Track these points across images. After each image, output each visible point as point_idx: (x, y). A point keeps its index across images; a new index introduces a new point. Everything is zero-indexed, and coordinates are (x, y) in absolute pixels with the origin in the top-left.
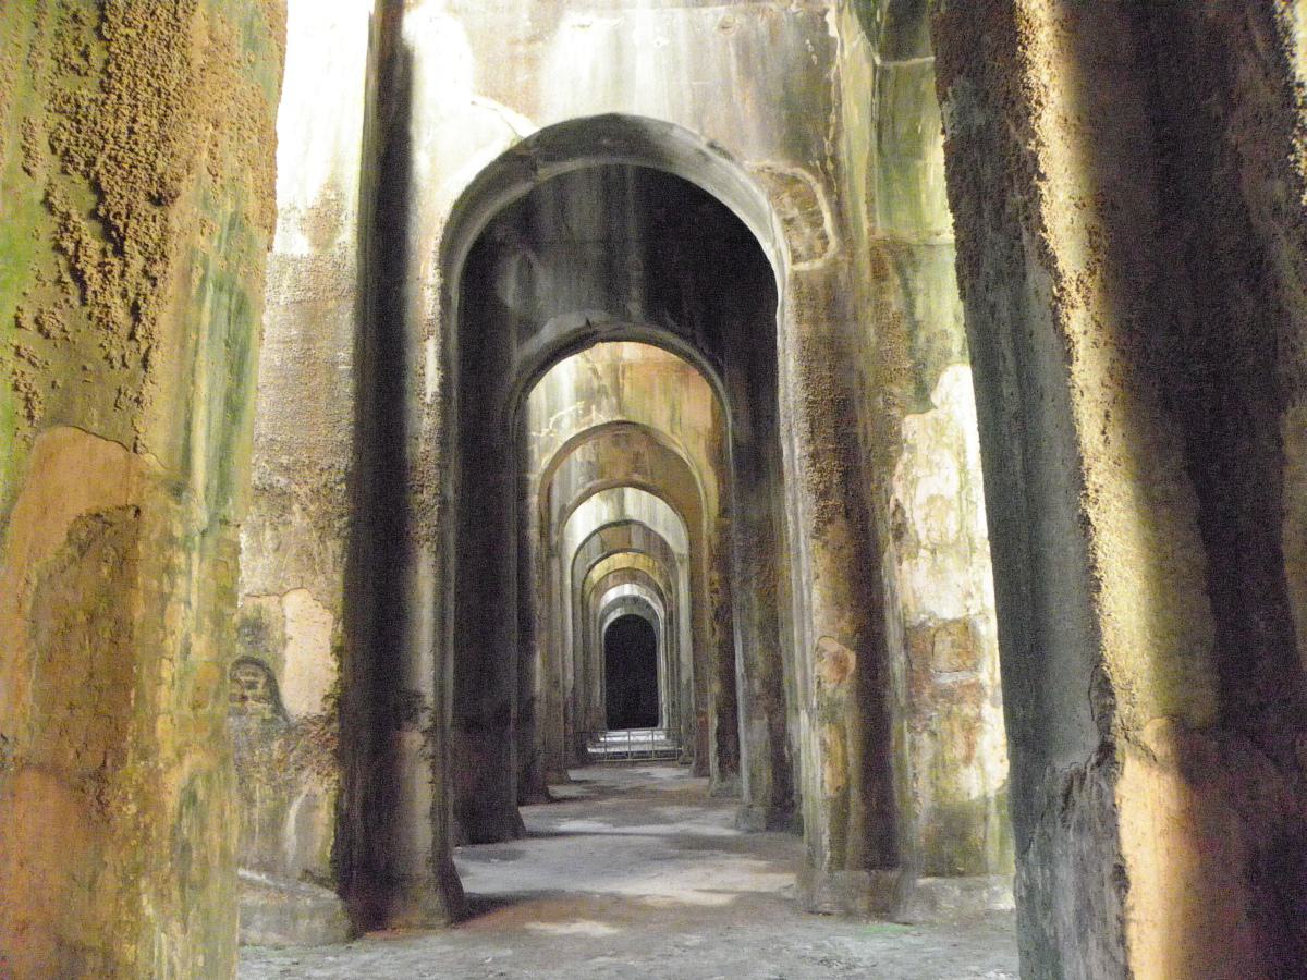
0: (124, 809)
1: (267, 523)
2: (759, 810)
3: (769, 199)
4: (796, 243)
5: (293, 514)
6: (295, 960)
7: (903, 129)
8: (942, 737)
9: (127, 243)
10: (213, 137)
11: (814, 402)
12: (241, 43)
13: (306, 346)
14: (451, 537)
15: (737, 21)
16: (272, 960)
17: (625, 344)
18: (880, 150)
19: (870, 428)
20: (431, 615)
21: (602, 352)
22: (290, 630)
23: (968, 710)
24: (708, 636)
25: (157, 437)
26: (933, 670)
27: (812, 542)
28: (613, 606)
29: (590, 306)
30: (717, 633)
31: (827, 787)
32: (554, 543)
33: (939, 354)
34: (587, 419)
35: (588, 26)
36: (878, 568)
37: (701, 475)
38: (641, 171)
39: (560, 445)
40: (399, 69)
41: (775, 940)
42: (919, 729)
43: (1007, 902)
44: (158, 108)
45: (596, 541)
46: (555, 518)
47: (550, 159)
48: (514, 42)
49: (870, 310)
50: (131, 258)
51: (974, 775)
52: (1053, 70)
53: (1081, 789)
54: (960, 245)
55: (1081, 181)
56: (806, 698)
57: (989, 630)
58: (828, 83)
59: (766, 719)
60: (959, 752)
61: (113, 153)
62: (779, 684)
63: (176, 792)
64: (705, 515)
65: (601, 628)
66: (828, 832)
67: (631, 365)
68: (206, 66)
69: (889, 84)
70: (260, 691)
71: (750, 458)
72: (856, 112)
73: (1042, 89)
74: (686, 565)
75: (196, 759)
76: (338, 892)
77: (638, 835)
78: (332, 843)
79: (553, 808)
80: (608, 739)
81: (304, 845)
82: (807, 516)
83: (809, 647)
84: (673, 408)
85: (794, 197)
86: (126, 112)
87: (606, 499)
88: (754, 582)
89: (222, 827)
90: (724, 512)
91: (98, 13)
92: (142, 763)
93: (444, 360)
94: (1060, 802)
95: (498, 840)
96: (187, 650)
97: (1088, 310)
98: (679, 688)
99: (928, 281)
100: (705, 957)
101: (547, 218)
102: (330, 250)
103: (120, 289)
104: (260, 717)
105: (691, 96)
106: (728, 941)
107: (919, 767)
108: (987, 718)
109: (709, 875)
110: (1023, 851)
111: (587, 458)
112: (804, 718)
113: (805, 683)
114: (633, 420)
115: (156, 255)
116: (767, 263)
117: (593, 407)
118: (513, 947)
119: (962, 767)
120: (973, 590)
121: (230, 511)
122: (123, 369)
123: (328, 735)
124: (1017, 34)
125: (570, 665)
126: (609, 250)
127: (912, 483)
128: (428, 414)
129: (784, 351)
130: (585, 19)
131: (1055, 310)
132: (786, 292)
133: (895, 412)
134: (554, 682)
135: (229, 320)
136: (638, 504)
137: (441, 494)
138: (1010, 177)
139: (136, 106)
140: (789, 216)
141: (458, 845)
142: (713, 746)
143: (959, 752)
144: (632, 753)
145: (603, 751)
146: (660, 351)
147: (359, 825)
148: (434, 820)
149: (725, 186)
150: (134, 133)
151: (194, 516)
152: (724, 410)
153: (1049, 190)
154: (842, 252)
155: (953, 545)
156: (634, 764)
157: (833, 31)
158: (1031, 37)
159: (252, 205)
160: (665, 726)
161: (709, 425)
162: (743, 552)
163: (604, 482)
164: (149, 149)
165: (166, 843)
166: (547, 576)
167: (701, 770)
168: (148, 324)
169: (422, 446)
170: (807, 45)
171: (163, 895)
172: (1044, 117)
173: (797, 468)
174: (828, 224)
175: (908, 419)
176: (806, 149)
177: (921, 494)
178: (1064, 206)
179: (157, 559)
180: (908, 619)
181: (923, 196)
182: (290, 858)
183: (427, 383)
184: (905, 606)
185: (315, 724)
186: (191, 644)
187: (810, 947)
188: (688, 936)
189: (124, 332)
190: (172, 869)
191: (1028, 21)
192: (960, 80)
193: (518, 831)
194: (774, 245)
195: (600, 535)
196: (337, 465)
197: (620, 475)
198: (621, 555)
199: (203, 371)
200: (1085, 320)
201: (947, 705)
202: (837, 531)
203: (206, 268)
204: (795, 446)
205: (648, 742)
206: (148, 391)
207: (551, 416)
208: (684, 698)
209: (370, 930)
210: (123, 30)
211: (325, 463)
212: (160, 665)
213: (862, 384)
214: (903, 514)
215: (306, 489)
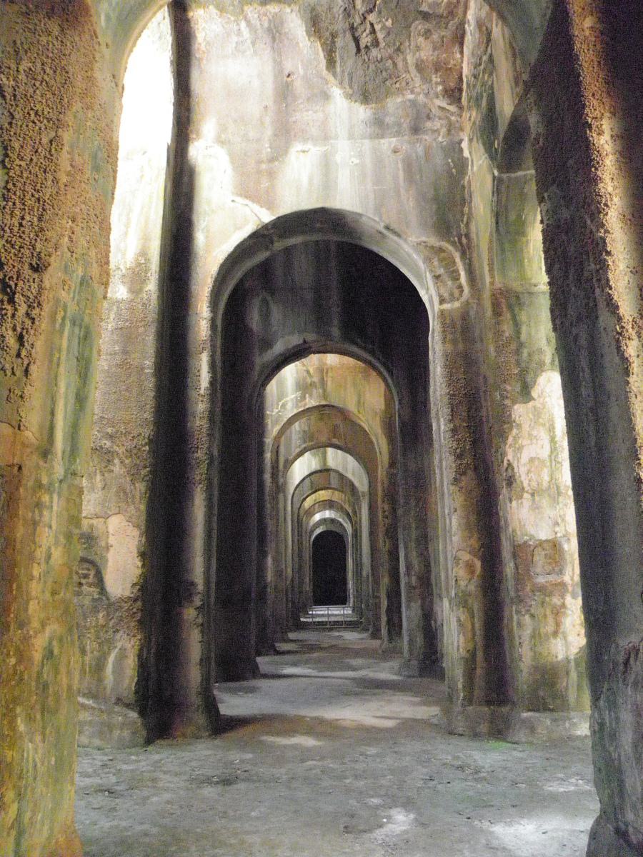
0: (8, 661)
1: (98, 471)
2: (414, 662)
3: (424, 263)
5: (114, 465)
6: (111, 758)
7: (512, 217)
8: (538, 618)
9: (16, 296)
10: (71, 228)
12: (90, 168)
13: (124, 357)
14: (216, 481)
15: (404, 147)
16: (95, 757)
17: (328, 355)
18: (497, 230)
20: (202, 531)
21: (313, 360)
22: (111, 540)
23: (556, 600)
25: (33, 420)
27: (452, 488)
31: (461, 650)
32: (280, 483)
34: (303, 403)
35: (307, 152)
38: (340, 245)
39: (285, 420)
40: (186, 179)
43: (583, 729)
44: (38, 210)
45: (307, 481)
47: (281, 236)
48: (260, 162)
49: (490, 335)
50: (19, 306)
51: (560, 644)
52: (616, 183)
53: (636, 660)
54: (553, 296)
55: (634, 256)
56: (447, 590)
57: (572, 547)
58: (463, 187)
60: (550, 628)
61: (10, 239)
62: (428, 579)
63: (40, 650)
64: (380, 467)
65: (310, 538)
68: (68, 184)
69: (503, 188)
70: (91, 579)
71: (410, 429)
73: (608, 196)
74: (367, 498)
75: (53, 628)
77: (334, 678)
79: (277, 658)
80: (314, 612)
81: (118, 681)
82: (448, 470)
83: (449, 557)
84: (359, 396)
85: (441, 260)
86: (18, 213)
87: (314, 455)
88: (413, 512)
89: (68, 672)
90: (392, 464)
91: (4, 152)
92: (20, 631)
93: (212, 366)
94: (621, 668)
95: (244, 679)
96: (49, 557)
97: (640, 341)
99: (529, 318)
101: (279, 271)
102: (140, 296)
103: (12, 325)
104: (91, 597)
106: (396, 752)
108: (569, 606)
109: (381, 706)
110: (596, 699)
112: (446, 603)
113: (447, 583)
115: (35, 303)
117: (307, 395)
118: (253, 752)
119: (552, 638)
120: (559, 521)
121: (79, 466)
122: (12, 376)
124: (591, 160)
127: (518, 449)
128: (202, 401)
129: (434, 362)
130: (306, 147)
131: (618, 341)
132: (436, 323)
133: (507, 402)
134: (279, 573)
135: (79, 343)
136: (335, 458)
138: (587, 253)
139: (25, 209)
140: (437, 274)
141: (217, 682)
142: (384, 618)
143: (550, 628)
144: (330, 622)
146: (351, 359)
150: (23, 226)
151: (55, 471)
152: (393, 398)
153: (613, 262)
156: (331, 630)
157: (466, 154)
158: (601, 162)
159: (95, 271)
162: (404, 491)
163: (314, 444)
164: (32, 236)
165: (33, 684)
167: (376, 634)
168: (29, 348)
169: (198, 422)
171: (30, 718)
172: (610, 214)
173: (442, 439)
175: (516, 407)
177: (525, 457)
178: (623, 273)
179: (32, 498)
180: (515, 539)
182: (108, 691)
183: (202, 381)
185: (126, 602)
186: (51, 554)
187: (450, 758)
189: (14, 352)
190: (36, 701)
191: (598, 152)
192: (554, 188)
193: (255, 673)
194: (427, 293)
195: (310, 478)
197: (323, 439)
198: (323, 492)
199: (63, 377)
200: (637, 347)
202: (469, 480)
203: (65, 312)
204: (441, 424)
205: (341, 615)
206: (28, 390)
208: (364, 587)
209: (158, 738)
210: (17, 162)
211: (135, 433)
212: (32, 567)
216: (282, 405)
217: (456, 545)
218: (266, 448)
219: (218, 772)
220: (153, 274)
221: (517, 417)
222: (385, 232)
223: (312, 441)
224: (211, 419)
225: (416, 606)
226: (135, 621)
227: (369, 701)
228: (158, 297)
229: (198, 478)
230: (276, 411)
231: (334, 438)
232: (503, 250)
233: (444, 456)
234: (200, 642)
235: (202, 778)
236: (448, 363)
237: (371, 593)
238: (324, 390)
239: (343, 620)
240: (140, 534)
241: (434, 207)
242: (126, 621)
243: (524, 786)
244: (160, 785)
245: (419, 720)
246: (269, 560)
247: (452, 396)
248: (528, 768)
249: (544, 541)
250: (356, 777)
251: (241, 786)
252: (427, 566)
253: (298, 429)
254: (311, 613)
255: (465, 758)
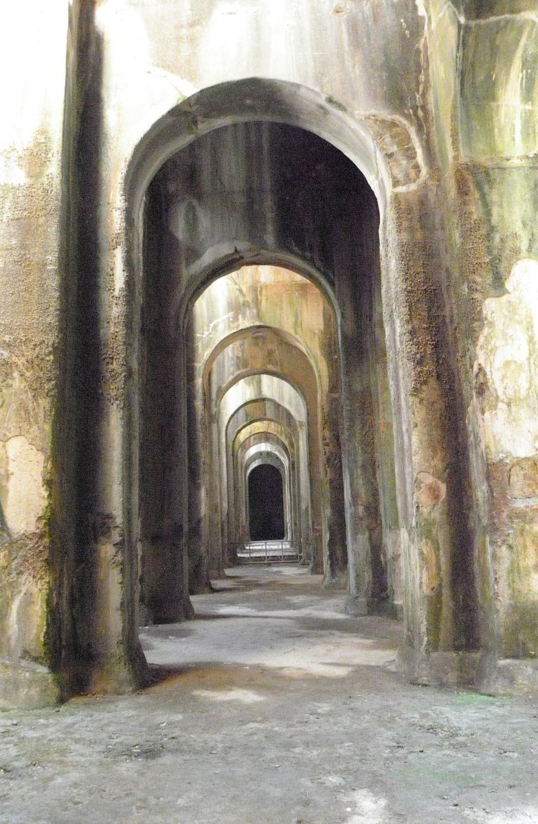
2: (362, 600)
3: (374, 140)
4: (396, 171)
5: (13, 379)
6: (15, 722)
7: (481, 77)
11: (412, 292)
13: (23, 253)
14: (136, 398)
19: (455, 311)
20: (120, 456)
21: (247, 271)
24: (322, 475)
26: (509, 498)
27: (411, 399)
28: (253, 458)
29: (236, 238)
30: (328, 474)
31: (424, 587)
33: (510, 251)
34: (236, 324)
35: (235, 13)
36: (463, 419)
37: (316, 362)
39: (217, 342)
40: (93, 49)
41: (387, 708)
42: (499, 544)
46: (214, 396)
47: (207, 116)
49: (455, 219)
56: (406, 518)
58: (418, 51)
59: (367, 534)
66: (425, 623)
67: (266, 286)
69: (471, 40)
71: (356, 345)
72: (443, 69)
76: (49, 667)
78: (44, 630)
79: (216, 596)
80: (251, 548)
81: (23, 632)
82: (406, 379)
83: (408, 480)
84: (296, 316)
85: (393, 137)
90: (333, 388)
93: (129, 263)
95: (177, 622)
98: (299, 513)
100: (335, 724)
102: (40, 180)
105: (313, 63)
107: (500, 573)
111: (236, 354)
112: (404, 534)
114: (268, 325)
116: (372, 193)
117: (240, 316)
118: (184, 711)
123: (41, 548)
125: (226, 498)
126: (249, 197)
128: (116, 304)
129: (387, 255)
134: (214, 508)
136: (272, 387)
137: (127, 364)
140: (389, 152)
142: (326, 553)
145: (248, 555)
147: (66, 617)
148: (123, 611)
149: (338, 134)
154: (431, 177)
155: (524, 399)
156: (269, 565)
157: (422, 11)
160: (289, 539)
161: (322, 327)
162: (348, 415)
163: (248, 371)
166: (209, 437)
167: (317, 569)
169: (112, 329)
170: (402, 23)
173: (398, 343)
174: (420, 158)
175: (488, 301)
176: (402, 100)
177: (499, 360)
180: (489, 457)
181: (496, 130)
182: (13, 642)
183: (116, 281)
184: (487, 447)
185: (31, 539)
187: (417, 716)
188: (319, 705)
194: (377, 177)
195: (246, 410)
196: (46, 341)
201: (521, 524)
202: (431, 390)
205: (279, 550)
207: (211, 322)
209: (72, 697)
211: (37, 340)
213: (449, 277)
214: (485, 375)
215: (23, 360)
216: (213, 328)
217: (416, 467)
218: (197, 372)
219: (140, 740)
220: (55, 154)
221: (489, 314)
222: (328, 106)
223: (246, 367)
224: (128, 325)
225: (363, 538)
226: (42, 561)
227: (313, 644)
228: (61, 181)
229: (113, 393)
230: (206, 333)
231: (269, 363)
232: (469, 118)
233: (400, 363)
234: (121, 583)
235: (120, 748)
236: (404, 254)
237: (311, 526)
238: (259, 311)
239: (281, 554)
240: (46, 458)
241: (385, 75)
242: (31, 560)
243: (516, 755)
244: (69, 758)
245: (373, 667)
246: (203, 493)
247: (409, 292)
248: (514, 730)
249: (523, 459)
250: (307, 744)
251: (167, 759)
252: (375, 494)
253: (231, 355)
254: (248, 548)
255: (434, 716)
